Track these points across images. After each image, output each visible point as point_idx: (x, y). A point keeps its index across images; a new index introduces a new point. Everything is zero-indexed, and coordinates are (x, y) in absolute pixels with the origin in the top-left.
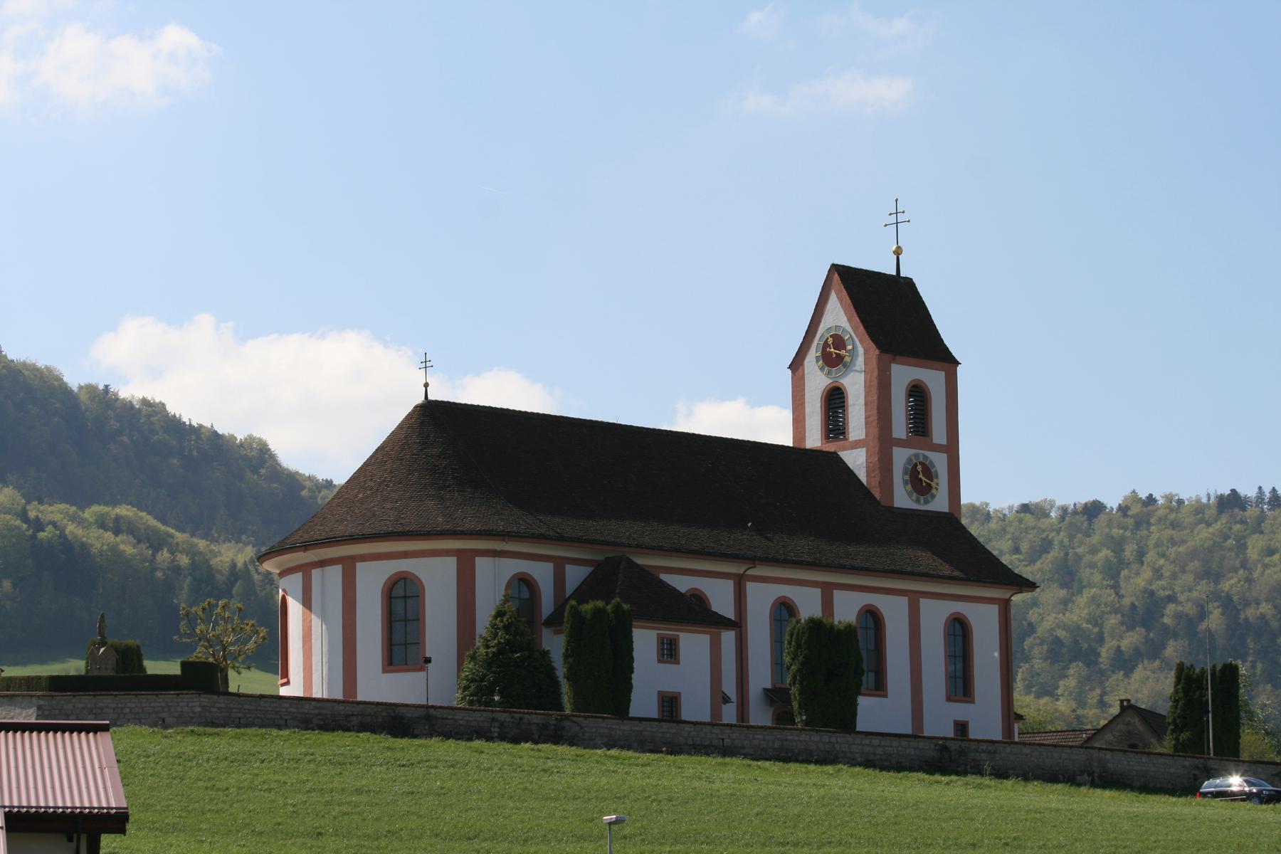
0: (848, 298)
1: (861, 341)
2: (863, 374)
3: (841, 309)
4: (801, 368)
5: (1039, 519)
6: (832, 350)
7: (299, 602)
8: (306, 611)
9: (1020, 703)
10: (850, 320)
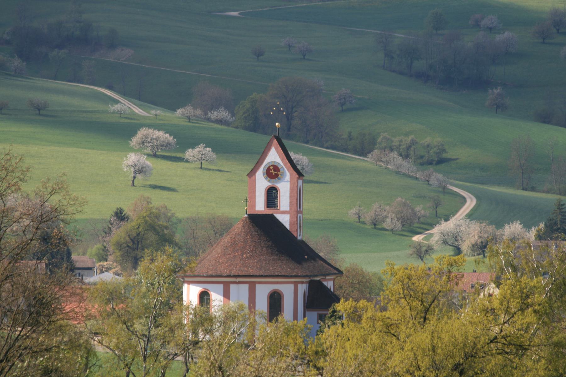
0: (282, 151)
1: (288, 170)
2: (289, 183)
3: (277, 155)
4: (253, 177)
5: (429, 240)
6: (273, 172)
7: (221, 295)
8: (226, 300)
9: (296, 160)
10: (282, 160)
